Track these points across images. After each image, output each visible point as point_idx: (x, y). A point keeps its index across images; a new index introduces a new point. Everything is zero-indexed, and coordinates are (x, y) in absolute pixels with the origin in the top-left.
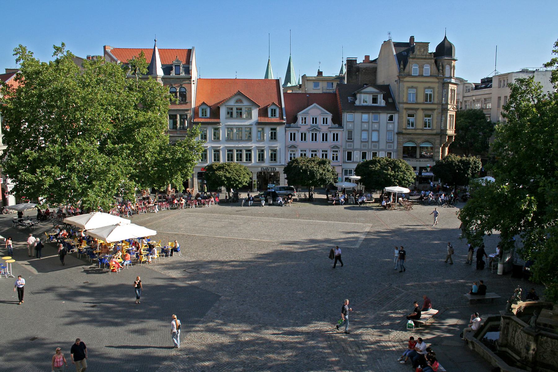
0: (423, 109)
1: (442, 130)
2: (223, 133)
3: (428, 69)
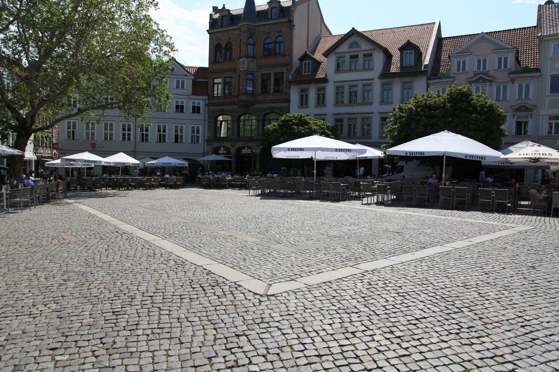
2: (330, 90)
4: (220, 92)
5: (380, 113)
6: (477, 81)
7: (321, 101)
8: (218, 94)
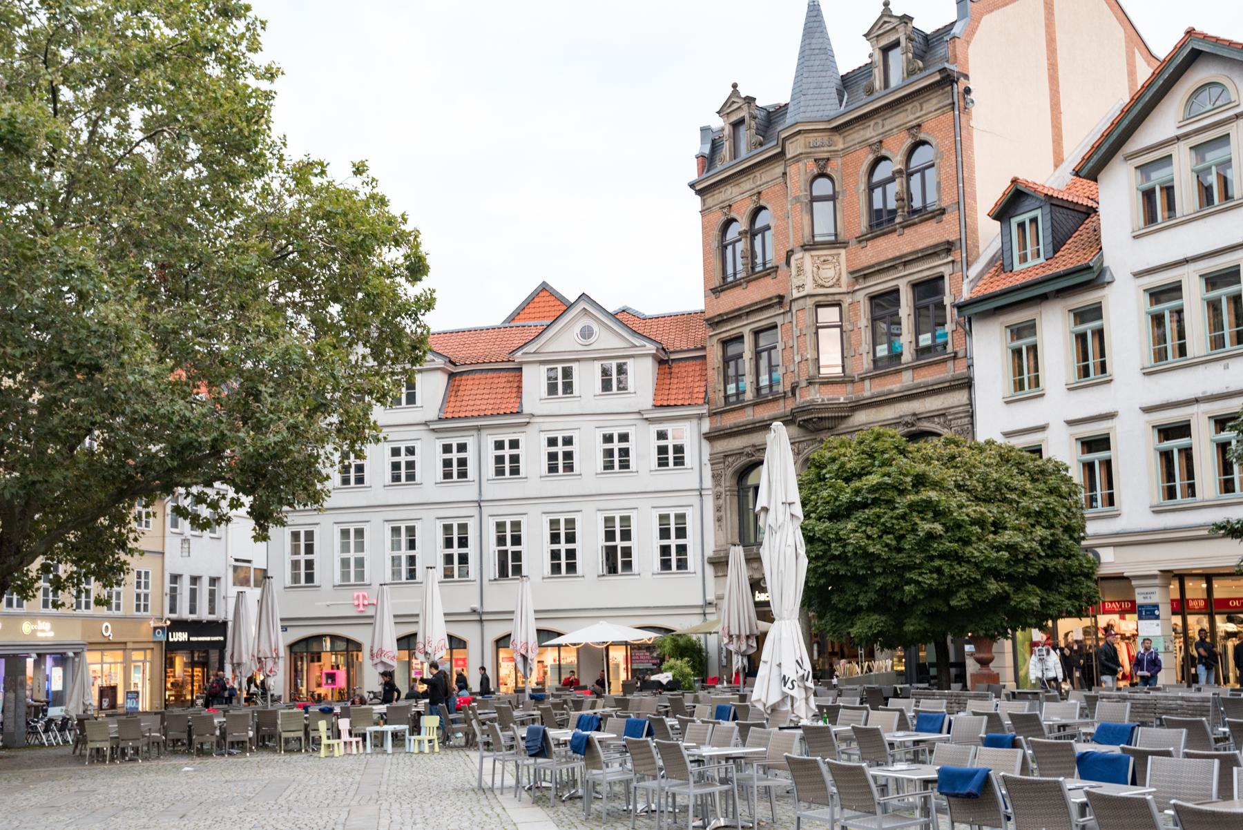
2: (1125, 314)
4: (740, 267)
5: (1147, 410)
7: (1091, 360)
8: (735, 274)
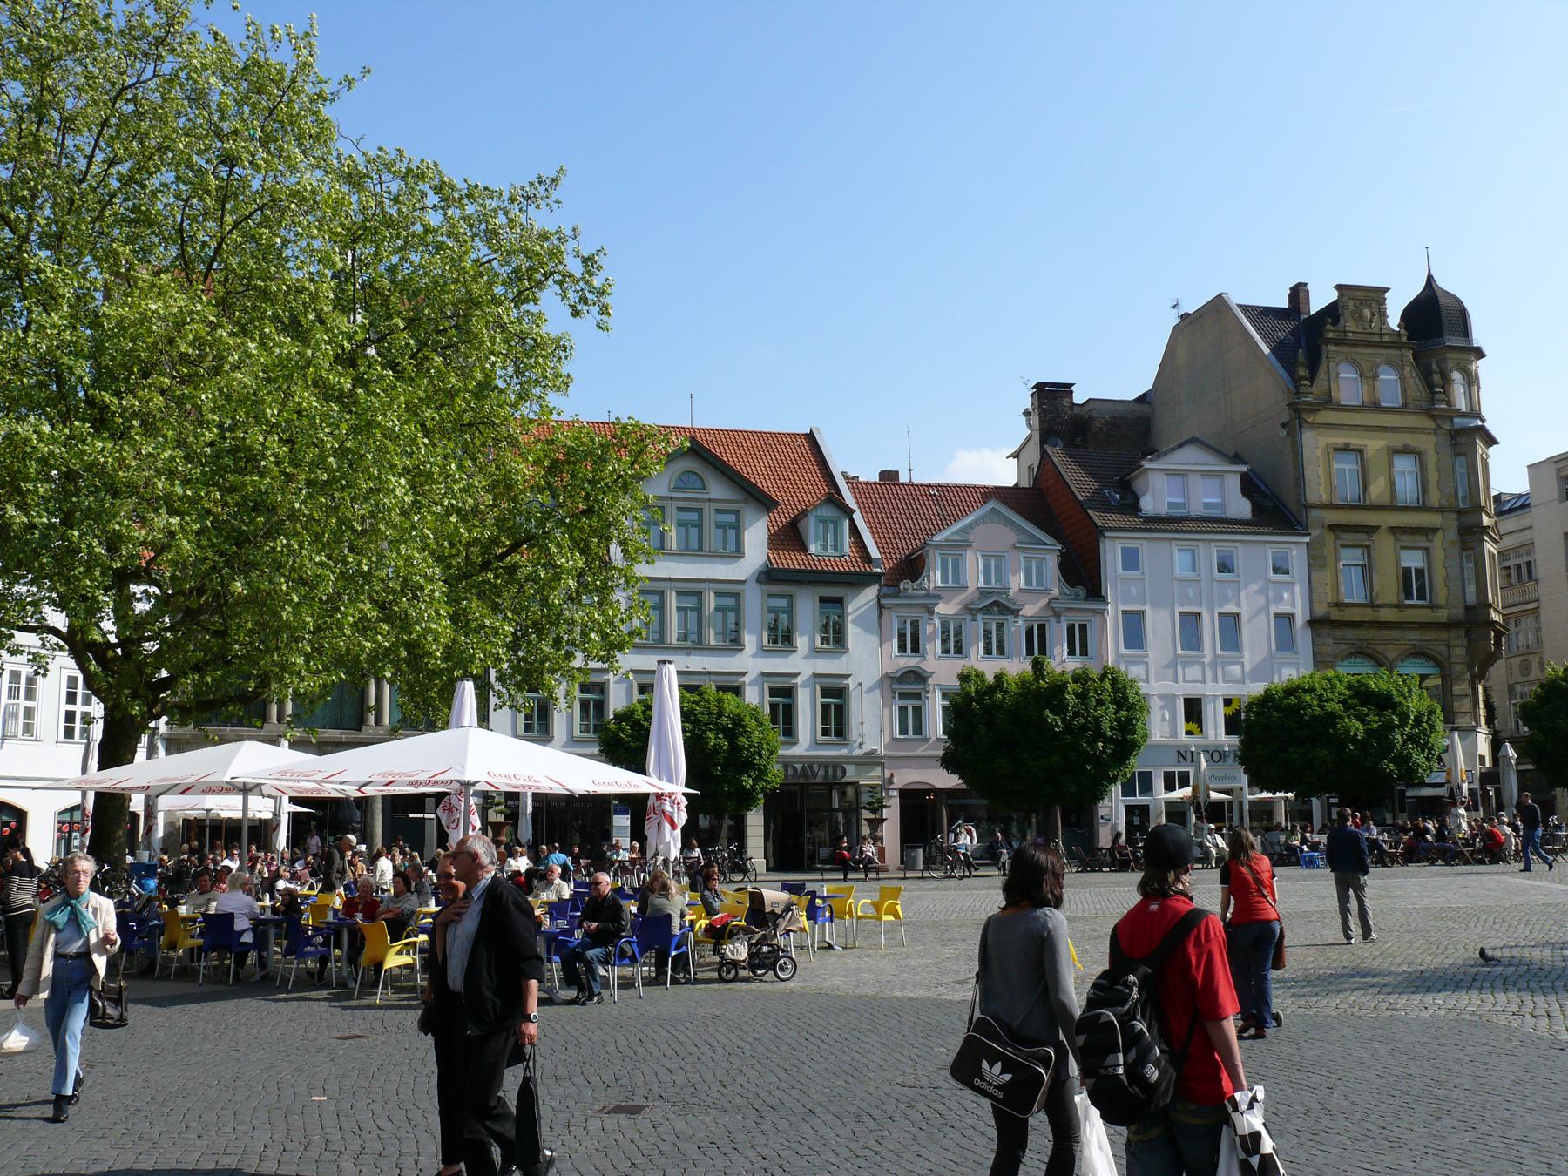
0: (1393, 530)
1: (1468, 609)
3: (1390, 384)
6: (987, 610)
